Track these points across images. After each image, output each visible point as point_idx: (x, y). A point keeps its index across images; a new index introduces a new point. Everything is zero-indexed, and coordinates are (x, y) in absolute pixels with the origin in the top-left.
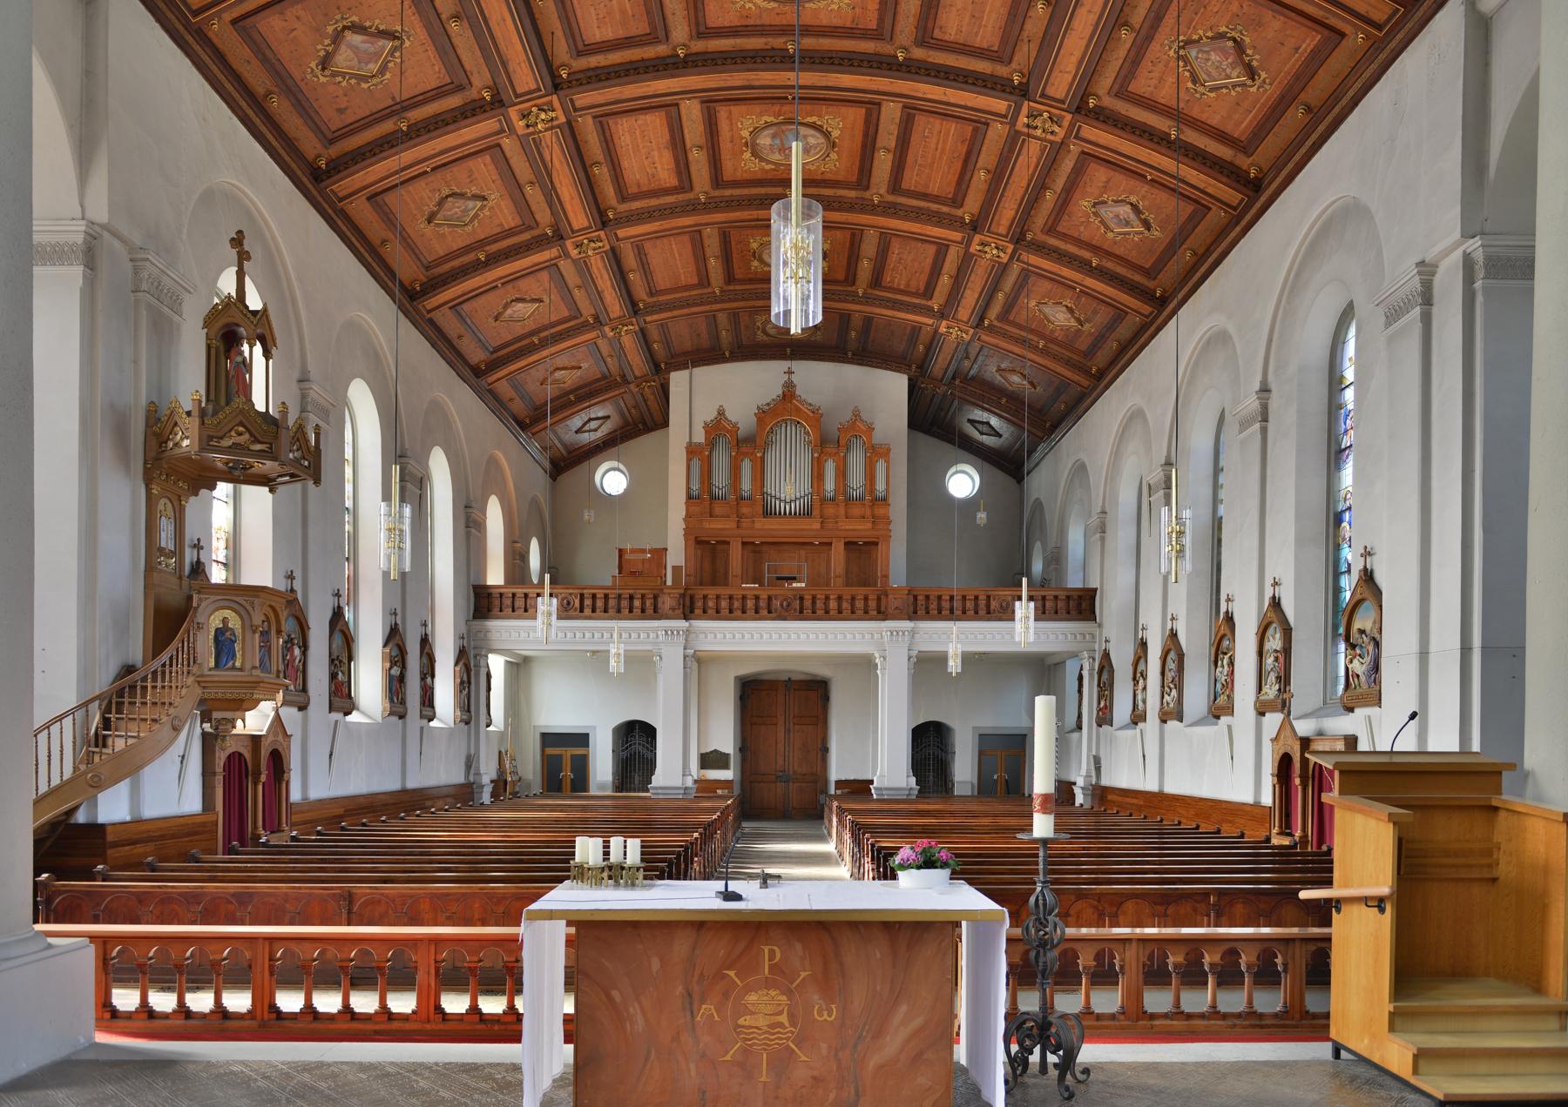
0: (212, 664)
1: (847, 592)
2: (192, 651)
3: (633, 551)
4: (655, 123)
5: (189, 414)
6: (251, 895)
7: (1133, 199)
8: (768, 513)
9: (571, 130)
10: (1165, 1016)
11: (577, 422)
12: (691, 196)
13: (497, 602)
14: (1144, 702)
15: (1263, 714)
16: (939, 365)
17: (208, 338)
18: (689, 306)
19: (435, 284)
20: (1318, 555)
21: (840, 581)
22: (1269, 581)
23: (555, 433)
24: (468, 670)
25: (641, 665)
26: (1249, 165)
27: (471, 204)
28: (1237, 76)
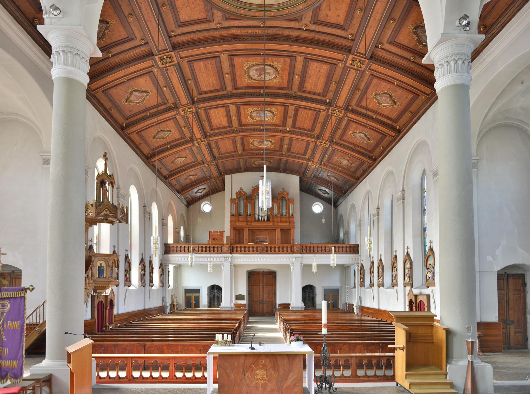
0: (97, 276)
2: (92, 273)
3: (214, 232)
4: (222, 111)
5: (92, 205)
6: (117, 345)
7: (364, 132)
8: (256, 220)
9: (197, 114)
10: (363, 377)
11: (196, 190)
13: (172, 249)
16: (309, 174)
19: (153, 155)
20: (419, 240)
21: (279, 241)
22: (406, 247)
25: (217, 267)
26: (397, 126)
27: (166, 133)
28: (391, 103)
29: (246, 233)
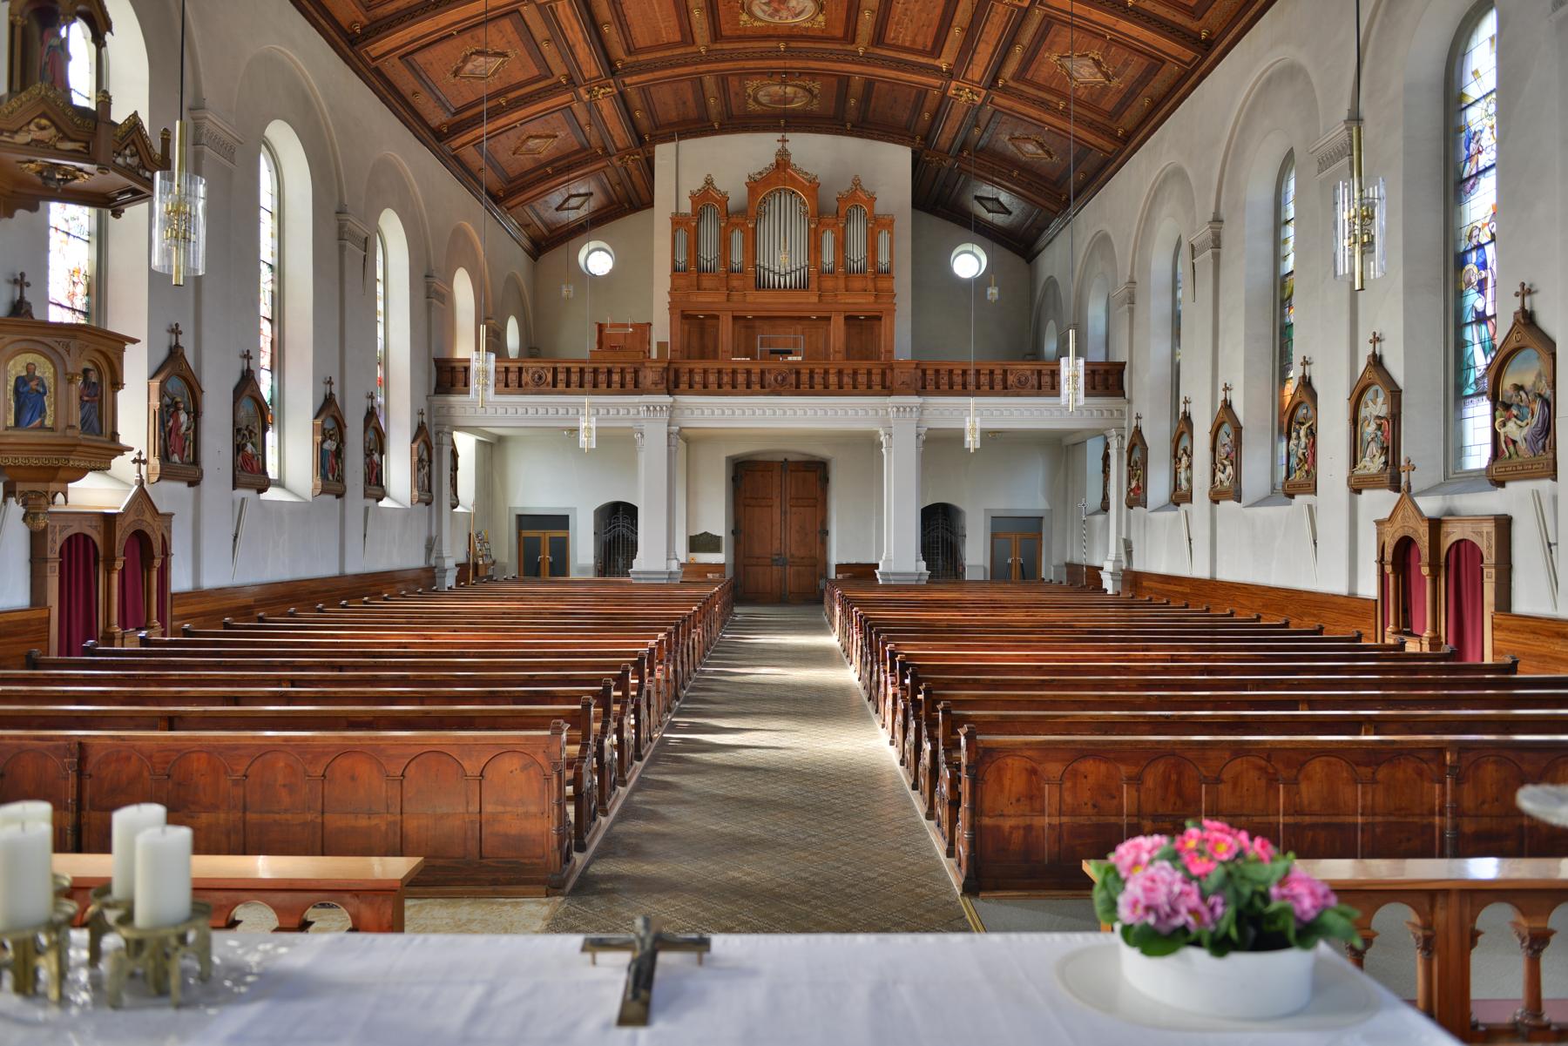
0: (11, 422)
1: (848, 366)
3: (612, 326)
8: (760, 285)
11: (556, 198)
12: (693, 49)
14: (1189, 481)
15: (1359, 491)
16: (946, 135)
17: (11, 13)
18: (672, 66)
20: (1433, 306)
21: (839, 356)
22: (1221, 386)
23: (534, 210)
24: (429, 448)
29: (726, 328)
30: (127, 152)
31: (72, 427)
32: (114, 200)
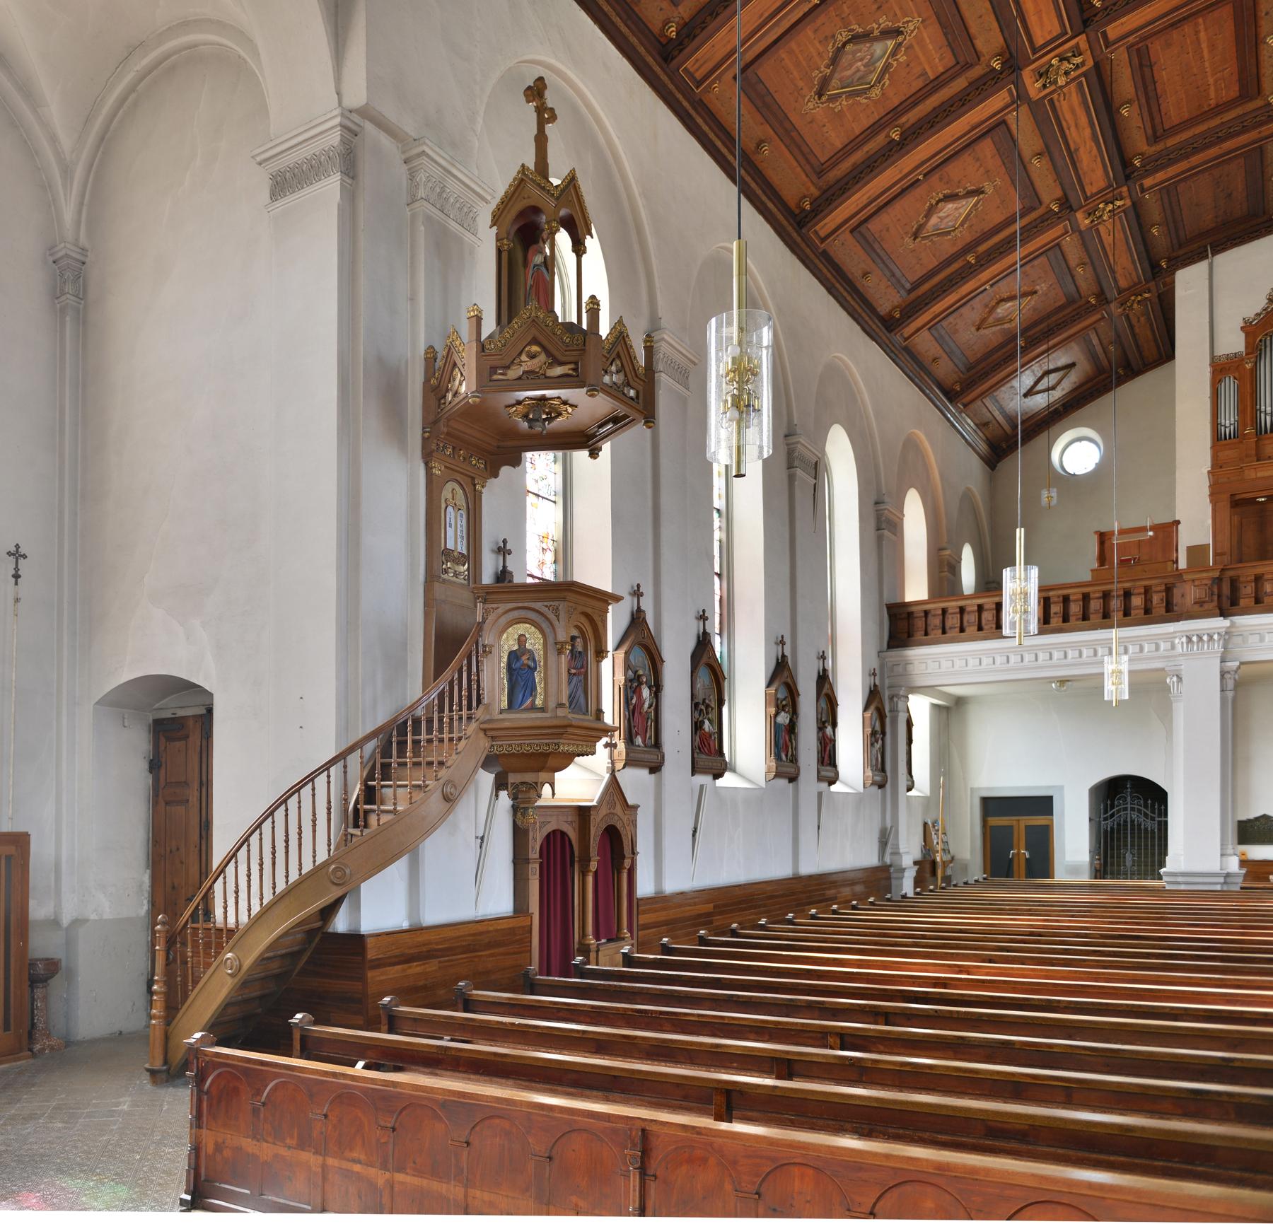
0: (505, 704)
13: (920, 623)
18: (1221, 140)
24: (881, 715)
27: (878, 48)
30: (613, 368)
31: (561, 705)
32: (594, 436)
